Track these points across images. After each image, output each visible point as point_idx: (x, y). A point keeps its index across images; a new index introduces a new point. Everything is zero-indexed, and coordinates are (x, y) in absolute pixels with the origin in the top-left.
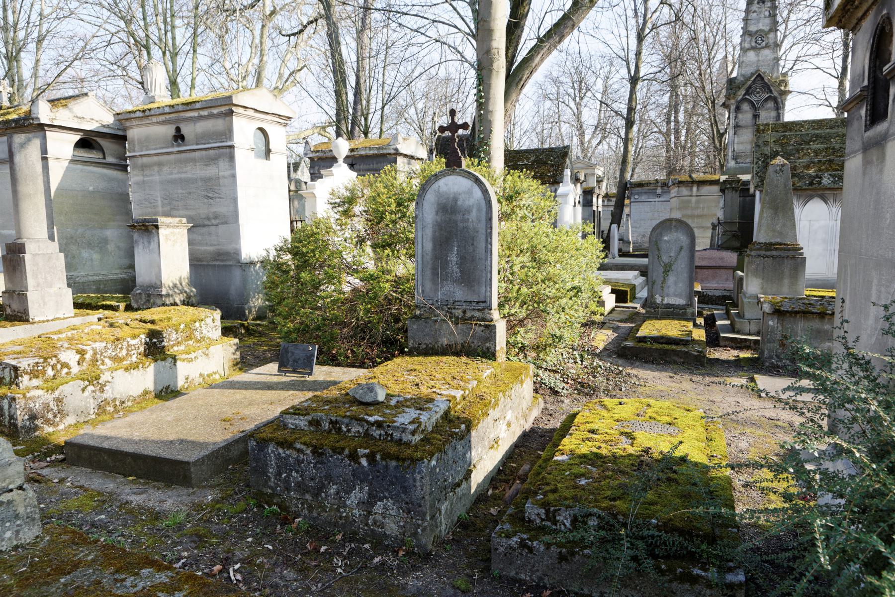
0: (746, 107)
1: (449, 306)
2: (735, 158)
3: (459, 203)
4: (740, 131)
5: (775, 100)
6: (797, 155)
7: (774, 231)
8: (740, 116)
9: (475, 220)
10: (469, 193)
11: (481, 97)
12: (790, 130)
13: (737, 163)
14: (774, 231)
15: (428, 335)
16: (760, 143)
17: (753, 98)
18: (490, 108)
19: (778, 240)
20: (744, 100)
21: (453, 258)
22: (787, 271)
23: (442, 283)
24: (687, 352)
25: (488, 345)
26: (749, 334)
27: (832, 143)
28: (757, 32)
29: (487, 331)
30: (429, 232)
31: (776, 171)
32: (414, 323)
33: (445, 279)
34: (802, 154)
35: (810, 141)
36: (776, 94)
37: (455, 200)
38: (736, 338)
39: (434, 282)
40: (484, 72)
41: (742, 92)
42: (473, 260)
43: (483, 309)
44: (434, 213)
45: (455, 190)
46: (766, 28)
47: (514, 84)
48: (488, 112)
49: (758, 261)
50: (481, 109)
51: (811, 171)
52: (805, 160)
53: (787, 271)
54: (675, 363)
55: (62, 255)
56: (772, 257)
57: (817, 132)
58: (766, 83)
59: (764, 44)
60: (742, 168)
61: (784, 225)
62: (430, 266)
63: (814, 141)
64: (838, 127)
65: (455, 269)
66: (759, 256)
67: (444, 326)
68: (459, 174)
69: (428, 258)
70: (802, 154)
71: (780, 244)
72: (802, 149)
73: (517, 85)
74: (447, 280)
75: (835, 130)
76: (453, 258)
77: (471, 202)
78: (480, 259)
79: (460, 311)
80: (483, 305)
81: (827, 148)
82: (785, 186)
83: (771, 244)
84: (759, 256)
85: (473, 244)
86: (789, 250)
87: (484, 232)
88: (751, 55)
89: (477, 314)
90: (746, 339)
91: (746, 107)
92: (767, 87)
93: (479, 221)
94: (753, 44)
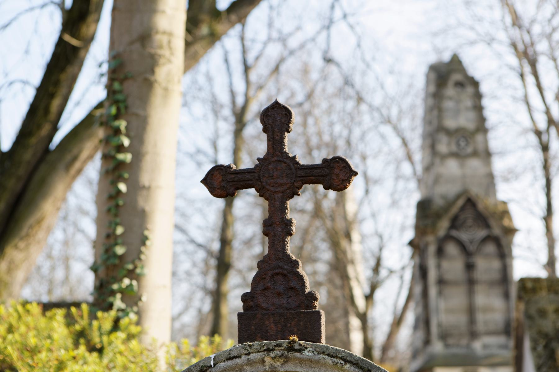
0: (452, 249)
2: (444, 336)
4: (448, 291)
5: (497, 241)
8: (445, 264)
13: (447, 346)
16: (533, 311)
17: (464, 236)
18: (145, 179)
20: (448, 237)
36: (497, 231)
40: (131, 88)
41: (444, 225)
48: (136, 187)
50: (120, 178)
55: (264, 136)
59: (469, 150)
88: (452, 167)
91: (452, 249)
92: (482, 219)
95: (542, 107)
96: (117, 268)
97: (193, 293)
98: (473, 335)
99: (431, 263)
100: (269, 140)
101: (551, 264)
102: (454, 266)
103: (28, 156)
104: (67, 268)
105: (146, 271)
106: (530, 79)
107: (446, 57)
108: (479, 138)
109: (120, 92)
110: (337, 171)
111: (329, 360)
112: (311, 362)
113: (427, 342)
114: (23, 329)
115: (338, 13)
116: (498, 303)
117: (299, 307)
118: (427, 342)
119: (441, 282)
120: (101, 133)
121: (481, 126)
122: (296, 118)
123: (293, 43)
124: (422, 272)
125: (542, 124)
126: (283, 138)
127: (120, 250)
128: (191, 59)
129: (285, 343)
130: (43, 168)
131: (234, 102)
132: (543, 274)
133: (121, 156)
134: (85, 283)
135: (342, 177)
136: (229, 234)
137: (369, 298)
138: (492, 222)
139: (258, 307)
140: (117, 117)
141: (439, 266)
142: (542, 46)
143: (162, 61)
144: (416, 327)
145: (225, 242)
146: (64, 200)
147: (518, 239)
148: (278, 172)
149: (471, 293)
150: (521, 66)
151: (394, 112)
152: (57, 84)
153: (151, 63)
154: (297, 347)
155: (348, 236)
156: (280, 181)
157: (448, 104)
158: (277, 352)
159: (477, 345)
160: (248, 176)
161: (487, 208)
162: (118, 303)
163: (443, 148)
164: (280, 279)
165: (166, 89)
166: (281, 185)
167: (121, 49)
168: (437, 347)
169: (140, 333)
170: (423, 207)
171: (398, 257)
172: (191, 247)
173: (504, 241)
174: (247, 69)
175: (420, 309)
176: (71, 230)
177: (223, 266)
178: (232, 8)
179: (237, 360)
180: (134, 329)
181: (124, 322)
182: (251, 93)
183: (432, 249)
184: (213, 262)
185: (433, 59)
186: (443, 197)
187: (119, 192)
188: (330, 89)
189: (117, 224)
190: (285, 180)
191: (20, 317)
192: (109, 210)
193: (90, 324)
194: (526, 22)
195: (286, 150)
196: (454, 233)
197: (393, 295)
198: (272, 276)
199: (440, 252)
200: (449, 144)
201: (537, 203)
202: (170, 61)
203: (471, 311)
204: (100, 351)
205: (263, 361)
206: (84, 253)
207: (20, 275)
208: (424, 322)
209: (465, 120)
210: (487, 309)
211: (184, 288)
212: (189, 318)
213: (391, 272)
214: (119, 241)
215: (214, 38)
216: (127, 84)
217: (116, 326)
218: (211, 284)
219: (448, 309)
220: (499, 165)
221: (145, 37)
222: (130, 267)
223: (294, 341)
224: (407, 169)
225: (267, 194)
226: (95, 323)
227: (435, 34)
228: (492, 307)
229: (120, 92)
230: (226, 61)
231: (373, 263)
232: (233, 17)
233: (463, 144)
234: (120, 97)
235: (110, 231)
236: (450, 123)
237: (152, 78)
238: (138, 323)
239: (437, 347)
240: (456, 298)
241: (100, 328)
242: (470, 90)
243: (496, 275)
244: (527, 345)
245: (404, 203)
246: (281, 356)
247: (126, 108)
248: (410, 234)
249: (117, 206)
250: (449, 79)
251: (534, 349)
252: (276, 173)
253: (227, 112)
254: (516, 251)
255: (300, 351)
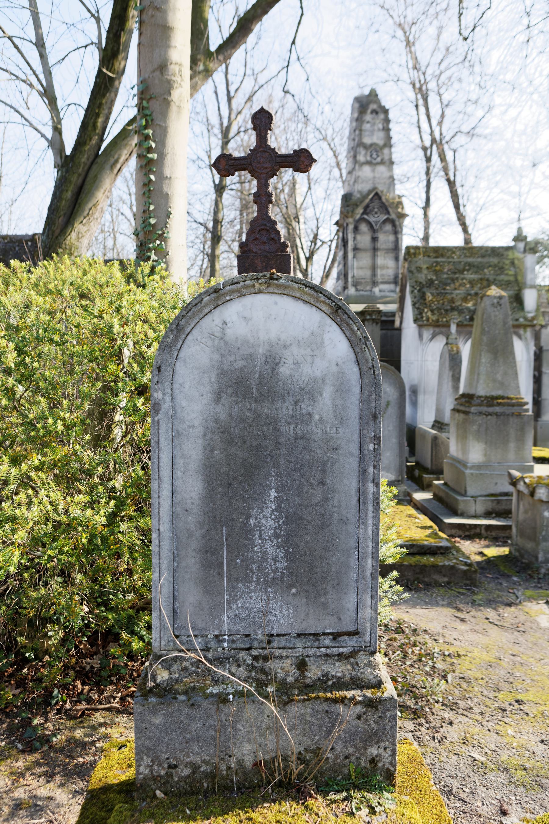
0: (364, 227)
1: (256, 654)
2: (355, 285)
3: (284, 370)
4: (360, 255)
5: (393, 222)
6: (452, 285)
7: (494, 381)
8: (359, 237)
9: (328, 416)
10: (315, 343)
11: (150, 150)
12: (442, 256)
13: (357, 290)
14: (494, 381)
15: (198, 739)
16: (413, 268)
18: (167, 172)
19: (500, 393)
20: (362, 219)
21: (266, 520)
22: (512, 432)
23: (232, 587)
24: (452, 568)
25: (373, 751)
26: (475, 517)
27: (485, 274)
28: (371, 145)
29: (372, 716)
30: (193, 450)
31: (493, 305)
32: (154, 711)
33: (242, 575)
34: (457, 284)
35: (464, 270)
36: (393, 216)
37: (273, 361)
38: (464, 525)
39: (209, 586)
40: (155, 105)
41: (360, 210)
42: (323, 525)
43: (354, 654)
44: (208, 397)
45: (273, 336)
46: (381, 143)
47: (108, 167)
48: (162, 178)
49: (480, 419)
50: (150, 171)
51: (470, 305)
52: (461, 291)
53: (512, 432)
54: (438, 585)
56: (496, 414)
57: (470, 260)
58: (383, 203)
59: (379, 159)
60: (362, 296)
61: (505, 374)
62: (195, 544)
63: (468, 270)
64: (489, 255)
65: (270, 548)
66: (480, 413)
67: (249, 711)
68: (284, 291)
69: (191, 521)
70: (457, 284)
71: (503, 398)
72: (457, 279)
73: (112, 168)
74: (246, 580)
75: (485, 260)
76: (266, 520)
77: (316, 369)
78: (343, 521)
79: (287, 664)
80: (352, 642)
81: (481, 279)
82: (505, 323)
83: (493, 398)
84: (480, 413)
85: (322, 483)
86: (513, 405)
87: (354, 448)
89: (338, 669)
90: (476, 526)
91: (364, 227)
92: (384, 208)
93: (342, 421)
94: (369, 158)
95: (429, 131)
96: (150, 236)
97: (197, 256)
98: (374, 283)
99: (350, 236)
100: (257, 136)
101: (426, 238)
102: (364, 239)
103: (84, 159)
104: (115, 239)
105: (170, 235)
106: (422, 110)
107: (367, 92)
108: (386, 151)
109: (147, 108)
110: (302, 159)
111: (295, 285)
112: (285, 287)
113: (345, 288)
114: (93, 272)
115: (294, 56)
116: (391, 263)
117: (277, 251)
118: (345, 288)
119: (355, 249)
120: (135, 140)
121: (388, 143)
122: (276, 120)
123: (262, 80)
124: (345, 242)
125: (428, 143)
126: (266, 135)
127: (153, 221)
128: (194, 88)
129: (268, 274)
130: (94, 167)
131: (222, 124)
132: (420, 244)
133: (150, 156)
134: (129, 248)
135: (306, 163)
136: (220, 216)
137: (309, 259)
138: (390, 210)
139: (250, 251)
140: (146, 127)
141: (355, 238)
142: (432, 85)
143: (175, 85)
144: (338, 279)
145: (217, 222)
146: (110, 191)
147: (407, 222)
148: (260, 162)
149: (374, 257)
150: (417, 99)
151: (330, 132)
152: (100, 106)
153: (168, 87)
154: (275, 277)
155: (297, 218)
156: (265, 165)
157: (366, 126)
158: (263, 280)
159: (376, 290)
160: (243, 162)
161: (387, 200)
162: (153, 257)
163: (361, 158)
164: (264, 233)
165: (179, 107)
166: (266, 168)
167: (147, 76)
168: (352, 291)
169: (168, 275)
170: (347, 199)
171: (328, 232)
172: (195, 225)
173: (397, 223)
174: (230, 99)
175: (341, 266)
176: (115, 213)
177: (216, 238)
178: (221, 48)
179: (238, 285)
180: (164, 273)
181: (158, 268)
182: (233, 116)
183: (351, 227)
184: (209, 235)
185: (357, 93)
186: (360, 192)
187: (150, 180)
188: (287, 115)
189: (150, 204)
190: (267, 165)
191: (90, 265)
192: (144, 194)
193: (136, 270)
194: (423, 63)
195: (269, 143)
196: (365, 217)
197: (322, 258)
198: (260, 231)
199: (356, 229)
200: (365, 155)
201: (420, 198)
202: (181, 86)
203: (374, 268)
204: (144, 287)
205: (254, 286)
206: (126, 226)
207: (85, 241)
208: (344, 275)
209: (377, 138)
210: (383, 267)
211: (192, 252)
212: (195, 271)
213: (323, 243)
214: (152, 215)
215: (208, 73)
216: (152, 102)
217: (152, 271)
218: (208, 250)
219: (359, 267)
220: (397, 171)
221: (163, 67)
222: (160, 232)
223: (273, 273)
224: (336, 172)
225: (256, 175)
226: (139, 269)
227: (360, 75)
228: (387, 266)
229: (147, 108)
230: (216, 92)
231: (312, 237)
232: (221, 57)
233: (374, 156)
234: (147, 112)
235: (146, 208)
236: (367, 140)
237: (169, 99)
238: (166, 270)
239: (352, 291)
240: (365, 260)
241: (142, 272)
242: (382, 116)
243: (391, 246)
244: (408, 289)
245: (333, 197)
246: (265, 283)
247: (152, 120)
248: (337, 217)
249: (150, 190)
250: (368, 107)
251: (412, 292)
252: (262, 160)
253: (217, 131)
254: (405, 230)
255: (277, 279)
